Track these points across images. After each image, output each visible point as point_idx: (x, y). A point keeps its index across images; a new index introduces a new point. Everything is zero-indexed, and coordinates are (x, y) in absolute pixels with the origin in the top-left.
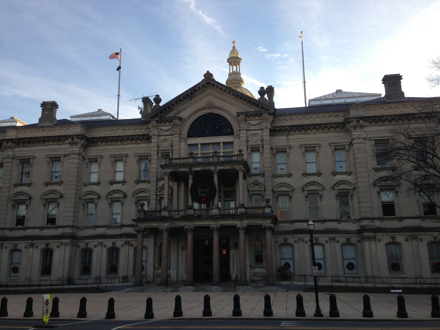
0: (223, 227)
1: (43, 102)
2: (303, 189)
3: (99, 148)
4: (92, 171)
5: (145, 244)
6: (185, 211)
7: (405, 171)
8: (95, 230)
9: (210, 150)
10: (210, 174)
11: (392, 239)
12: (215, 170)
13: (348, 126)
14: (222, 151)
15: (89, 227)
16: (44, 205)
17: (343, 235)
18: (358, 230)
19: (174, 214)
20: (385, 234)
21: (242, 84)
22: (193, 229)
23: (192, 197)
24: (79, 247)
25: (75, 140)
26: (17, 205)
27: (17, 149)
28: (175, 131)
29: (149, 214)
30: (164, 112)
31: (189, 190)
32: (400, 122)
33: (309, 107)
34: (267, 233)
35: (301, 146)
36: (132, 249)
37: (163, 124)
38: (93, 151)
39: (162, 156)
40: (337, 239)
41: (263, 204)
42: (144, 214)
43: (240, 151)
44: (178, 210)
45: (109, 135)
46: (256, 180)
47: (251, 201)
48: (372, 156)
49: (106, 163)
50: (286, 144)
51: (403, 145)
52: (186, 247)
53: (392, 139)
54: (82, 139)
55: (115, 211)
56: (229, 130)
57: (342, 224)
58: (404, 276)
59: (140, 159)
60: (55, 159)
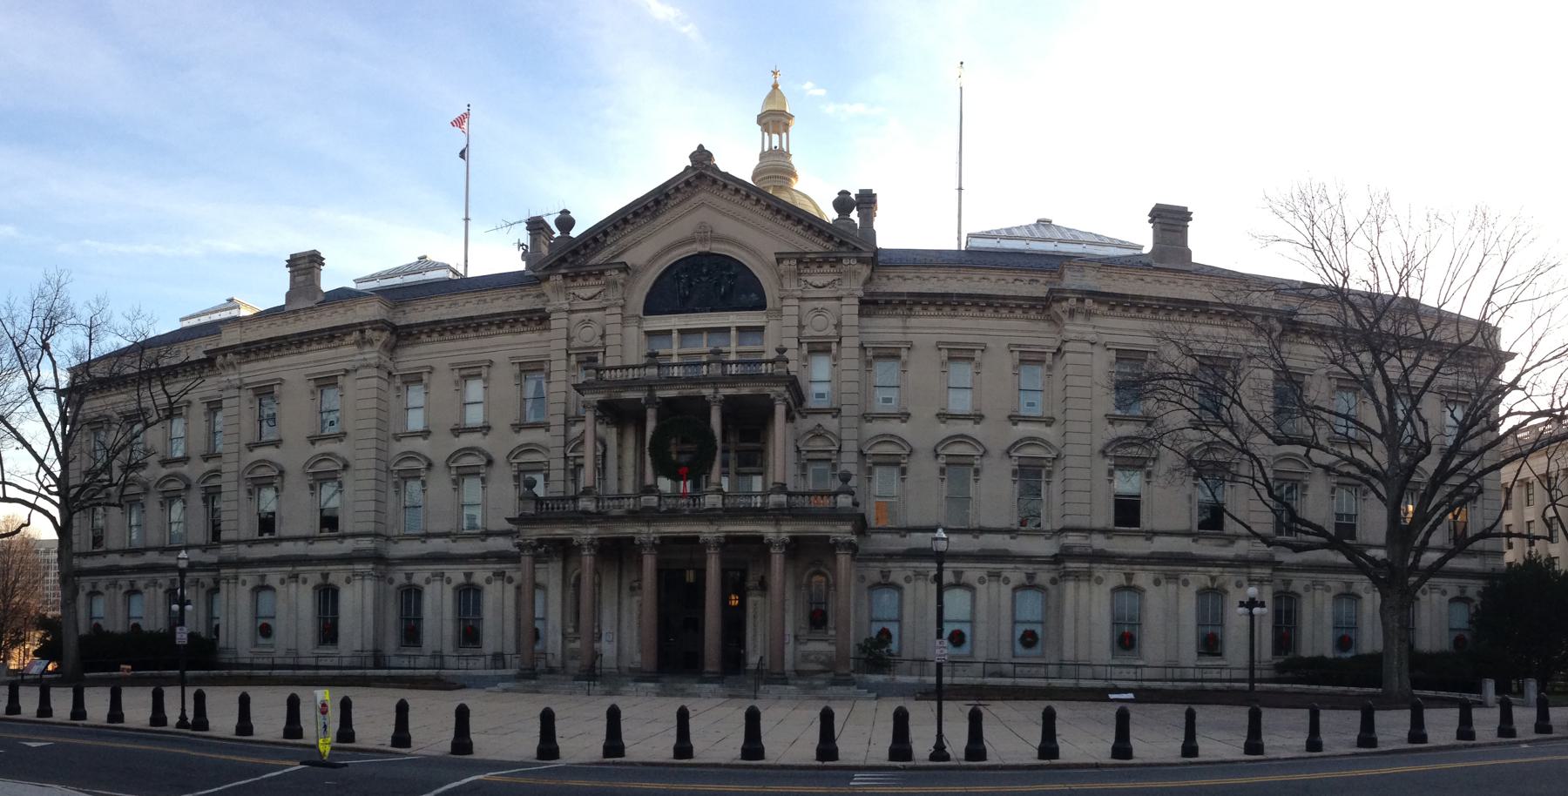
0: (732, 541)
1: (291, 255)
2: (935, 450)
3: (422, 349)
4: (410, 405)
5: (540, 578)
6: (637, 497)
7: (1170, 427)
8: (424, 542)
9: (703, 346)
10: (702, 405)
11: (883, 577)
12: (715, 397)
13: (1056, 308)
14: (733, 348)
15: (411, 535)
16: (312, 487)
17: (1018, 566)
18: (1056, 555)
19: (609, 507)
20: (1113, 566)
21: (793, 179)
22: (657, 542)
23: (654, 464)
24: (391, 581)
25: (368, 333)
26: (256, 489)
27: (245, 367)
28: (608, 300)
29: (547, 505)
30: (583, 252)
31: (647, 446)
32: (1175, 316)
33: (967, 251)
34: (839, 557)
35: (939, 346)
36: (510, 590)
37: (580, 281)
38: (412, 357)
39: (578, 362)
40: (1004, 574)
41: (835, 485)
42: (537, 504)
43: (781, 350)
44: (620, 497)
45: (445, 317)
46: (819, 425)
47: (804, 476)
48: (1103, 386)
49: (443, 381)
50: (900, 338)
51: (1172, 370)
52: (640, 588)
53: (1155, 353)
54: (383, 330)
55: (467, 500)
56: (753, 295)
57: (1020, 539)
58: (1141, 663)
59: (522, 371)
60: (326, 382)
